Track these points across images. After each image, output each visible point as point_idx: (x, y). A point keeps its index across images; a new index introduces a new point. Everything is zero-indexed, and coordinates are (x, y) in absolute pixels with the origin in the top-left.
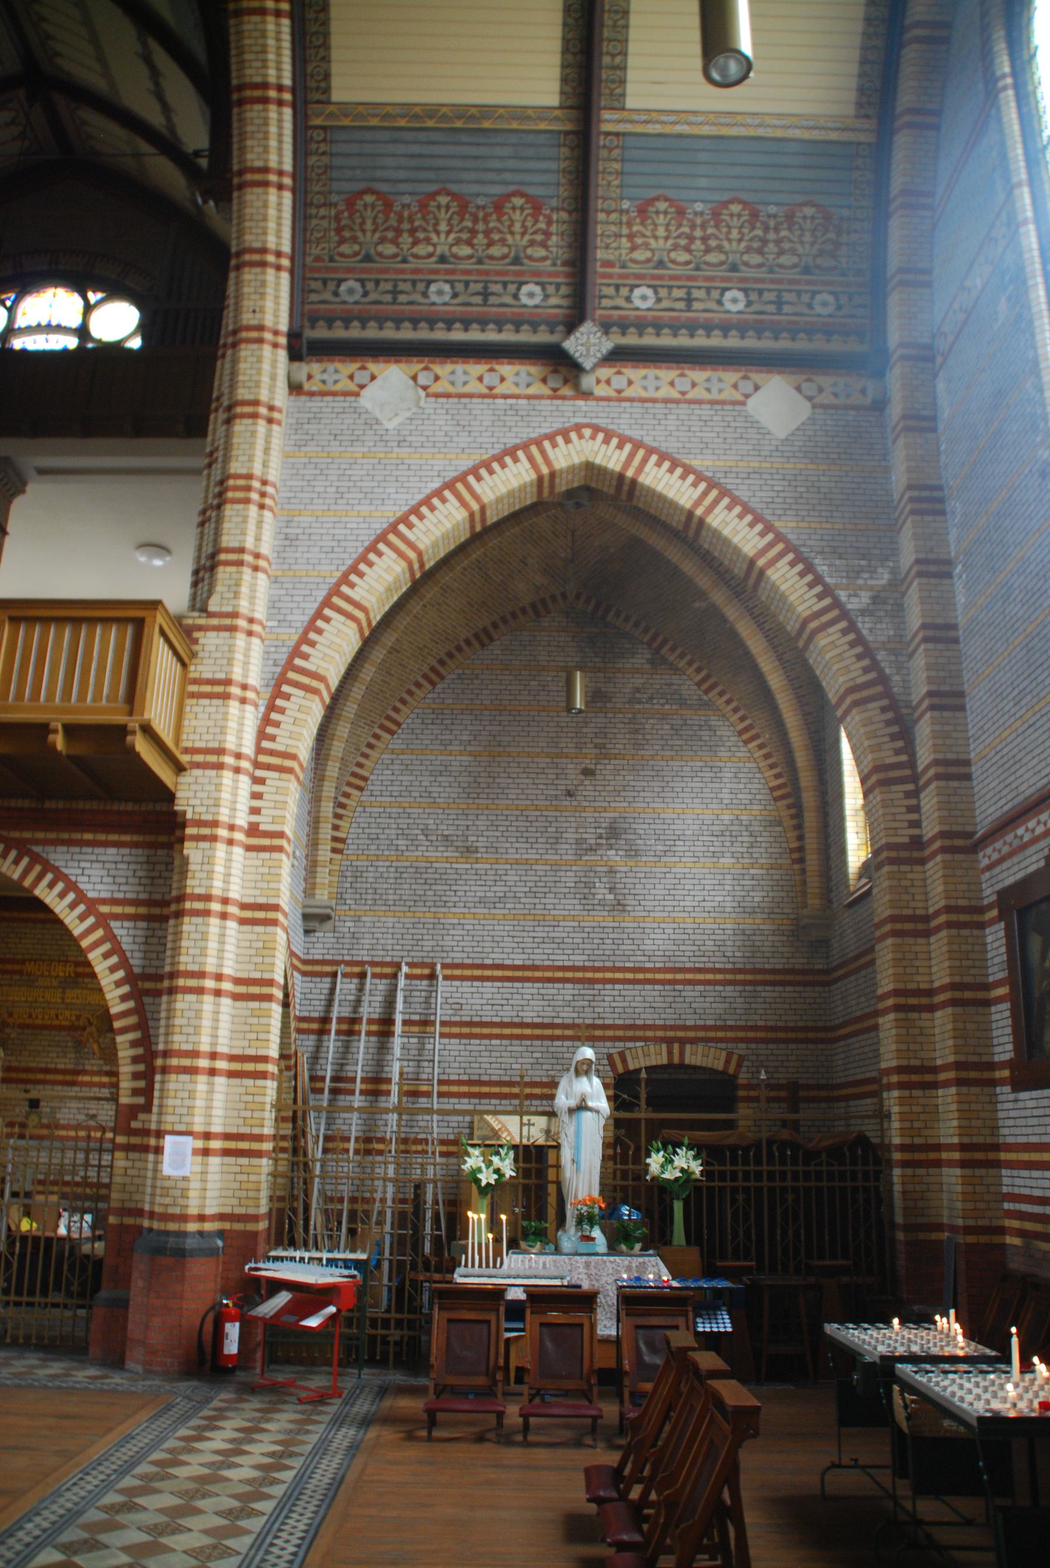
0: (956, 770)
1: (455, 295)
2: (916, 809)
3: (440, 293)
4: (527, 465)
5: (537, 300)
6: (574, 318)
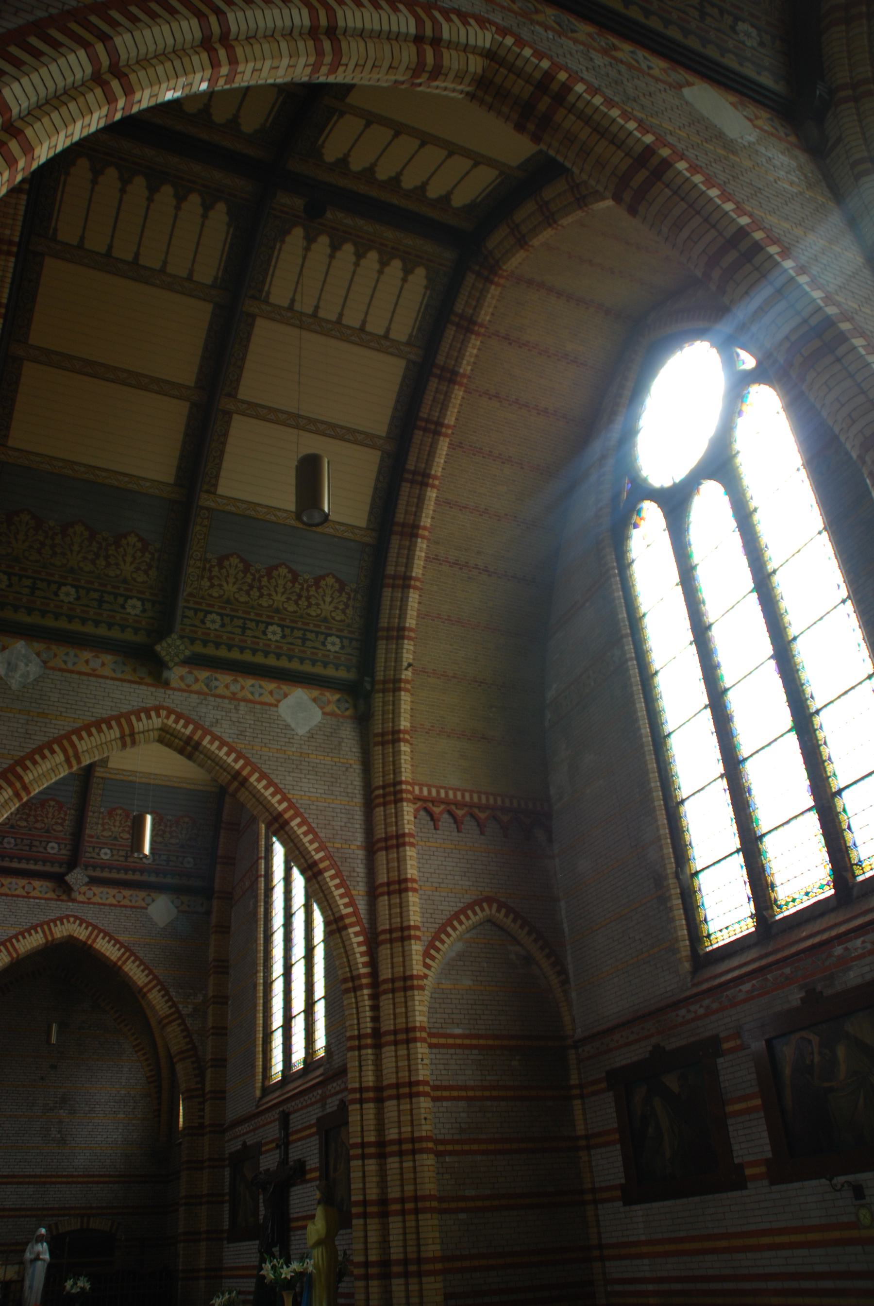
0: (220, 1095)
1: (16, 845)
2: (203, 1110)
3: (9, 843)
4: (42, 935)
5: (55, 851)
6: (72, 864)
